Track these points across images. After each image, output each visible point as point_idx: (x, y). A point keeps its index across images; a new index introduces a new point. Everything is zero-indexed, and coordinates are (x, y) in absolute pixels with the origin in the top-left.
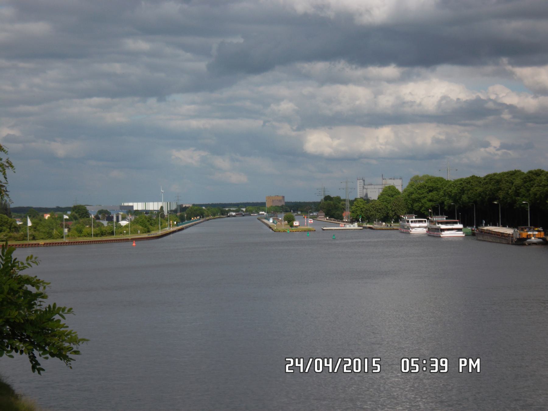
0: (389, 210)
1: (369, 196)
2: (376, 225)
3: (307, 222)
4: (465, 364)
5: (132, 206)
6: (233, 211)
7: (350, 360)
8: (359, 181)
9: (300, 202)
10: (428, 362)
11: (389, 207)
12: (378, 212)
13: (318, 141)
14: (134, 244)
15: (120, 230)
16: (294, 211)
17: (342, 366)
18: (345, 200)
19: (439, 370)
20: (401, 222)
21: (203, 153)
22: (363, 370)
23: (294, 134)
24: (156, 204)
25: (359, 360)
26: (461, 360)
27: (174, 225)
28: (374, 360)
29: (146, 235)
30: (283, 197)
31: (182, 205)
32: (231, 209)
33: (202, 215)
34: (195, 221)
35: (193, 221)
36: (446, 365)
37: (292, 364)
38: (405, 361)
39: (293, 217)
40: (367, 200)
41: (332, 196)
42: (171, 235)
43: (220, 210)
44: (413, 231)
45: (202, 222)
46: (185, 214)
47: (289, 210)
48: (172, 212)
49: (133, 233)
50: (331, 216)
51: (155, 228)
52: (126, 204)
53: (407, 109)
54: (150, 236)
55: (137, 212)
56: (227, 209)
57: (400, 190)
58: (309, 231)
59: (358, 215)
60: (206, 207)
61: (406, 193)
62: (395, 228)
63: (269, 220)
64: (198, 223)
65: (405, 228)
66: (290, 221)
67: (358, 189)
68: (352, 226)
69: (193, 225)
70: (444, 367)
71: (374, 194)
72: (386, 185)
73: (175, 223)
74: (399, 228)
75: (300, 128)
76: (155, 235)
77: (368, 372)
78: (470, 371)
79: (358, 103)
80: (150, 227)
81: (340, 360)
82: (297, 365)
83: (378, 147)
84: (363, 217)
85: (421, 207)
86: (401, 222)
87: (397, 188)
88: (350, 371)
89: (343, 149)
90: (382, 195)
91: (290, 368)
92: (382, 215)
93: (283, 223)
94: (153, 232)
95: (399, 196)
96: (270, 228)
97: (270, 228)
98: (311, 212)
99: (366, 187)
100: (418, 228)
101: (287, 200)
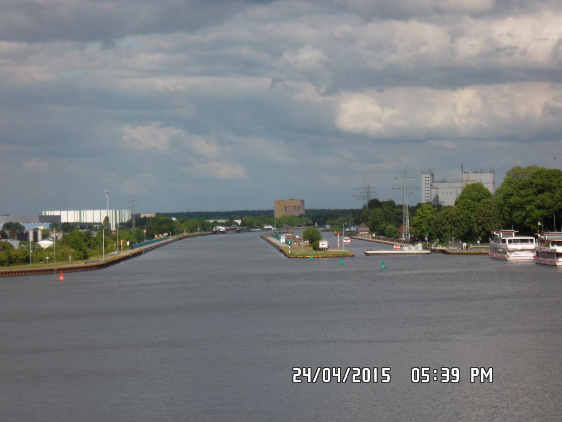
0: (473, 223)
1: (441, 200)
2: (452, 248)
3: (341, 241)
4: (477, 374)
5: (59, 217)
6: (222, 224)
7: (359, 370)
8: (423, 176)
9: (329, 210)
10: (439, 371)
11: (473, 217)
12: (455, 226)
13: (360, 112)
14: (61, 278)
15: (39, 255)
16: (320, 224)
17: (350, 375)
18: (401, 207)
19: (450, 380)
20: (492, 242)
21: (173, 131)
22: (372, 380)
23: (320, 99)
24: (97, 212)
25: (368, 369)
26: (473, 369)
27: (126, 247)
28: (384, 370)
29: (81, 264)
30: (303, 202)
31: (140, 214)
32: (219, 221)
33: (172, 231)
34: (161, 239)
35: (157, 241)
36: (457, 375)
37: (299, 374)
38: (416, 371)
39: (318, 233)
40: (437, 207)
41: (381, 200)
42: (122, 263)
43: (199, 223)
44: (512, 257)
45: (171, 242)
46: (146, 228)
47: (310, 222)
48: (123, 226)
49: (61, 260)
50: (381, 233)
51: (95, 252)
52: (49, 213)
53: (504, 60)
54: (88, 265)
55: (68, 227)
56: (212, 221)
57: (491, 190)
58: (344, 256)
59: (423, 231)
60: (177, 218)
61: (500, 196)
62: (483, 251)
63: (279, 239)
64: (165, 244)
65: (499, 252)
66: (313, 239)
67: (424, 189)
68: (413, 248)
69: (157, 247)
70: (456, 377)
71: (449, 197)
72: (469, 183)
73: (128, 243)
74: (488, 252)
75: (333, 90)
76: (95, 264)
77: (377, 382)
78: (482, 381)
79: (423, 49)
80: (88, 249)
81: (349, 369)
82: (304, 374)
83: (456, 120)
84: (430, 234)
85: (525, 218)
86: (492, 242)
87: (486, 186)
88: (359, 381)
89: (401, 123)
90: (461, 198)
91: (298, 378)
92: (461, 229)
93: (302, 243)
94: (92, 259)
95: (490, 200)
96: (281, 251)
97: (281, 251)
98: (346, 226)
99: (435, 185)
100: (521, 251)
101: (308, 206)
